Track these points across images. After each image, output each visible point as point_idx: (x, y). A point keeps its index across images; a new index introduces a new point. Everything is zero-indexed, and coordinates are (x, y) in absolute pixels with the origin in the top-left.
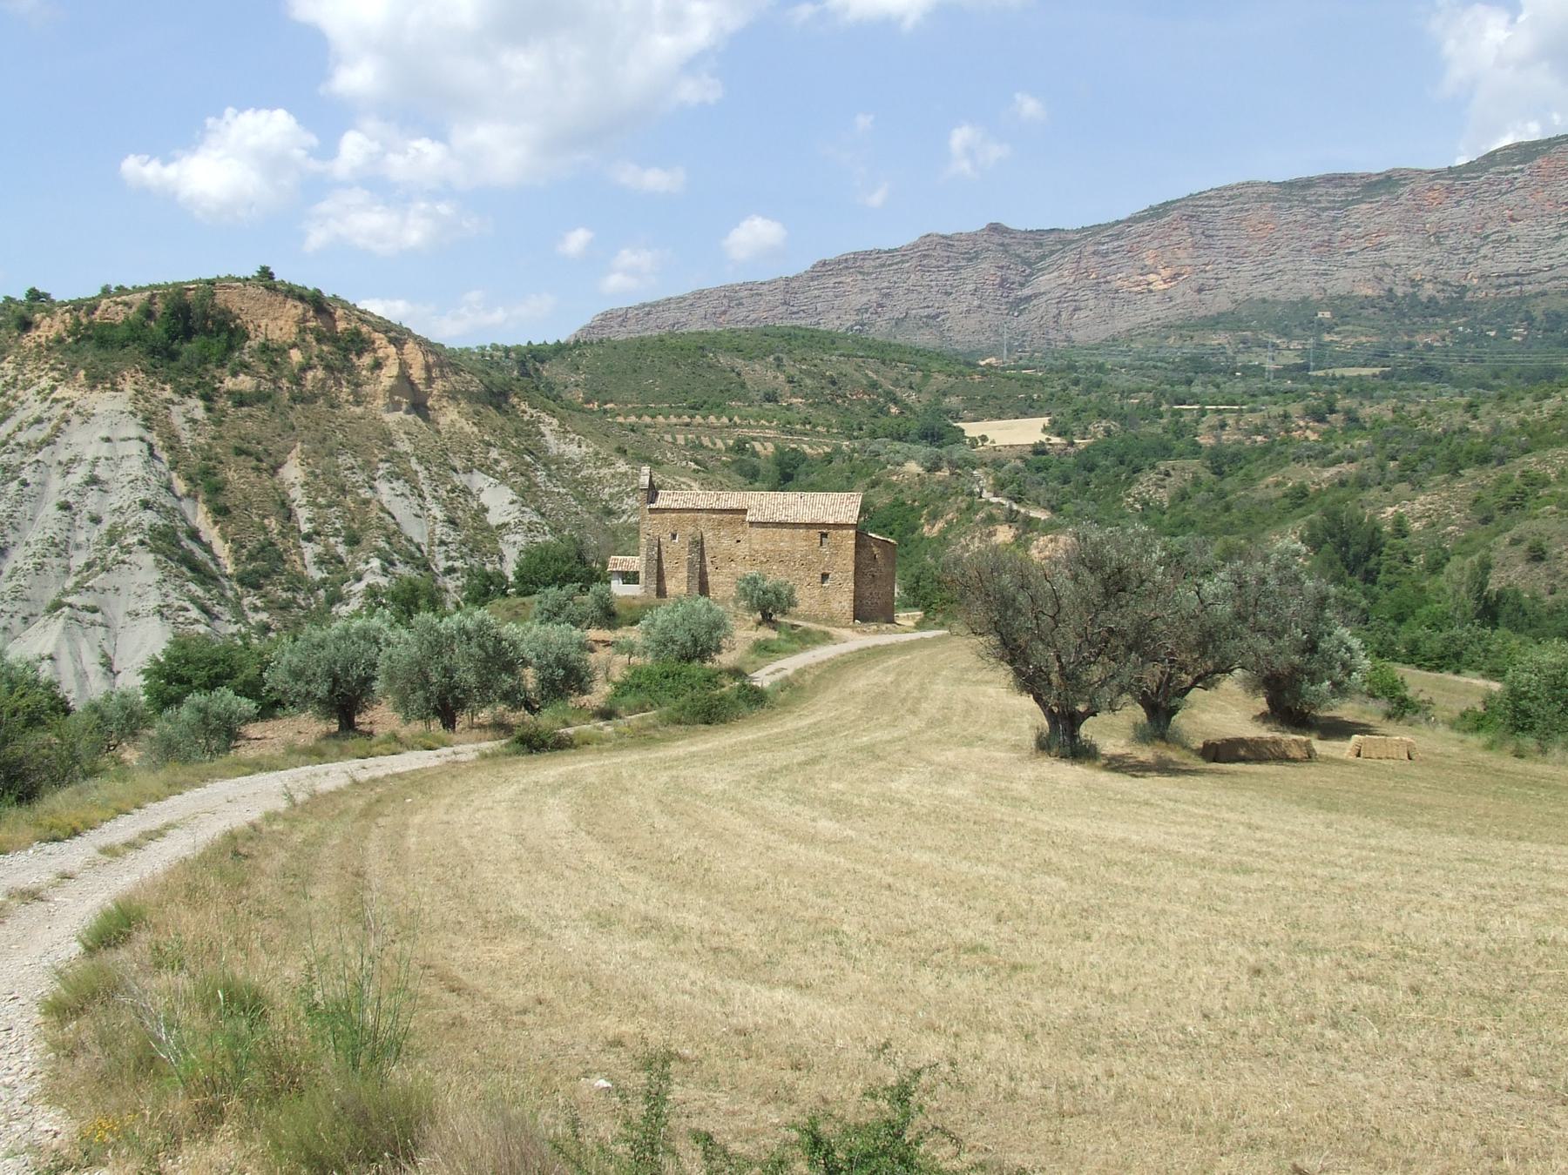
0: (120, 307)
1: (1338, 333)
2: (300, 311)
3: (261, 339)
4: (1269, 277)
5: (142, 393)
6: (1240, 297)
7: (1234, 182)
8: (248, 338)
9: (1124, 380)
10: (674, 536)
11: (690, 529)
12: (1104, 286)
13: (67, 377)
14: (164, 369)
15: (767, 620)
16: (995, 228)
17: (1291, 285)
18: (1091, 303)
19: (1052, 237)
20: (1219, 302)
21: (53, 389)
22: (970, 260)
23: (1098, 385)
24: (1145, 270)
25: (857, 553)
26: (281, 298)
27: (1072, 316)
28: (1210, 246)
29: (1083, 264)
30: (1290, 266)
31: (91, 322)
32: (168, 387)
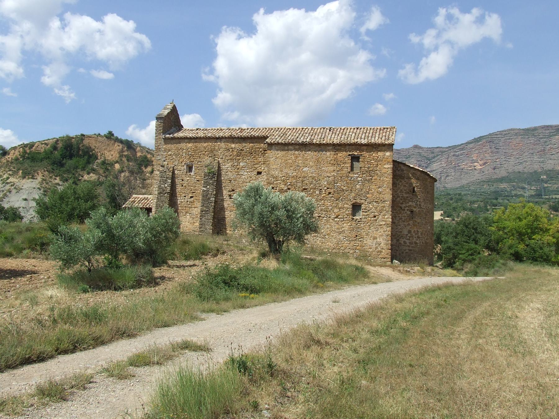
0: (43, 145)
1: (550, 183)
2: (121, 147)
3: (103, 159)
4: (521, 163)
5: (45, 180)
6: (510, 171)
7: (506, 129)
8: (97, 159)
9: (470, 198)
10: (190, 168)
11: (207, 160)
12: (457, 168)
13: (15, 173)
14: (58, 171)
15: (275, 248)
16: (416, 147)
17: (529, 166)
18: (453, 174)
19: (438, 150)
20: (502, 173)
21: (8, 178)
22: (407, 158)
23: (461, 200)
24: (473, 161)
25: (394, 184)
26: (113, 142)
27: (446, 178)
28: (498, 152)
29: (449, 160)
30: (529, 159)
31: (30, 152)
32: (58, 178)
